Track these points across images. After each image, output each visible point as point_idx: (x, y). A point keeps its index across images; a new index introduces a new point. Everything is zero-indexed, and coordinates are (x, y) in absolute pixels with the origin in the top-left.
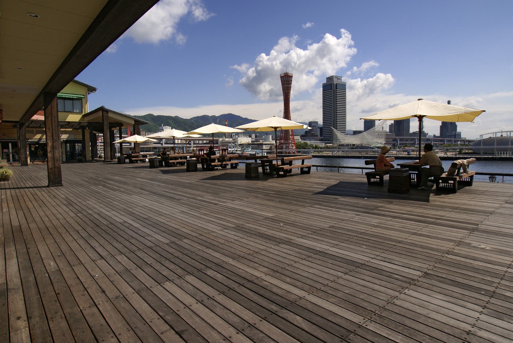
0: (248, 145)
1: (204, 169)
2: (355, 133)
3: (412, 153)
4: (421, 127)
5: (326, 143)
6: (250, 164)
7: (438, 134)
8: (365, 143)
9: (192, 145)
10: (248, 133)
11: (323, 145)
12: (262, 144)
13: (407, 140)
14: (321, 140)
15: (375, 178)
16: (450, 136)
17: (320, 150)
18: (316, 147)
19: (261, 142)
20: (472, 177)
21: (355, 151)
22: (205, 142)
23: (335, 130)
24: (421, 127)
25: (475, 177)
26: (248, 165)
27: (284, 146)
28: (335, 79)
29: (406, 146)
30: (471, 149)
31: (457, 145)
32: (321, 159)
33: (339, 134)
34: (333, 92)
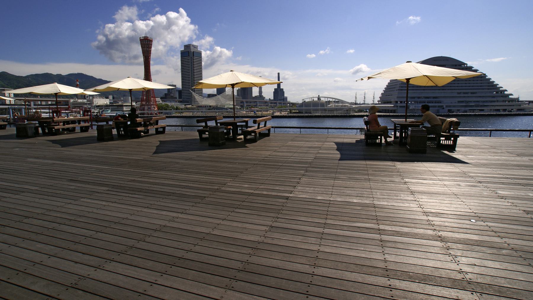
0: (107, 106)
1: (44, 134)
2: (210, 96)
3: (257, 113)
4: (260, 92)
5: (185, 105)
6: (102, 126)
7: (272, 98)
8: (219, 105)
9: (32, 106)
10: (104, 94)
11: (183, 106)
12: (122, 106)
13: (250, 103)
14: (181, 102)
15: (251, 135)
16: (280, 100)
17: (180, 111)
18: (177, 109)
19: (120, 103)
20: (269, 130)
21: (212, 112)
22: (50, 103)
23: (193, 93)
24: (260, 92)
25: (272, 130)
26: (99, 128)
27: (146, 108)
28: (192, 48)
29: (252, 107)
30: (297, 110)
31: (287, 107)
32: (180, 119)
33: (197, 97)
34: (190, 59)
